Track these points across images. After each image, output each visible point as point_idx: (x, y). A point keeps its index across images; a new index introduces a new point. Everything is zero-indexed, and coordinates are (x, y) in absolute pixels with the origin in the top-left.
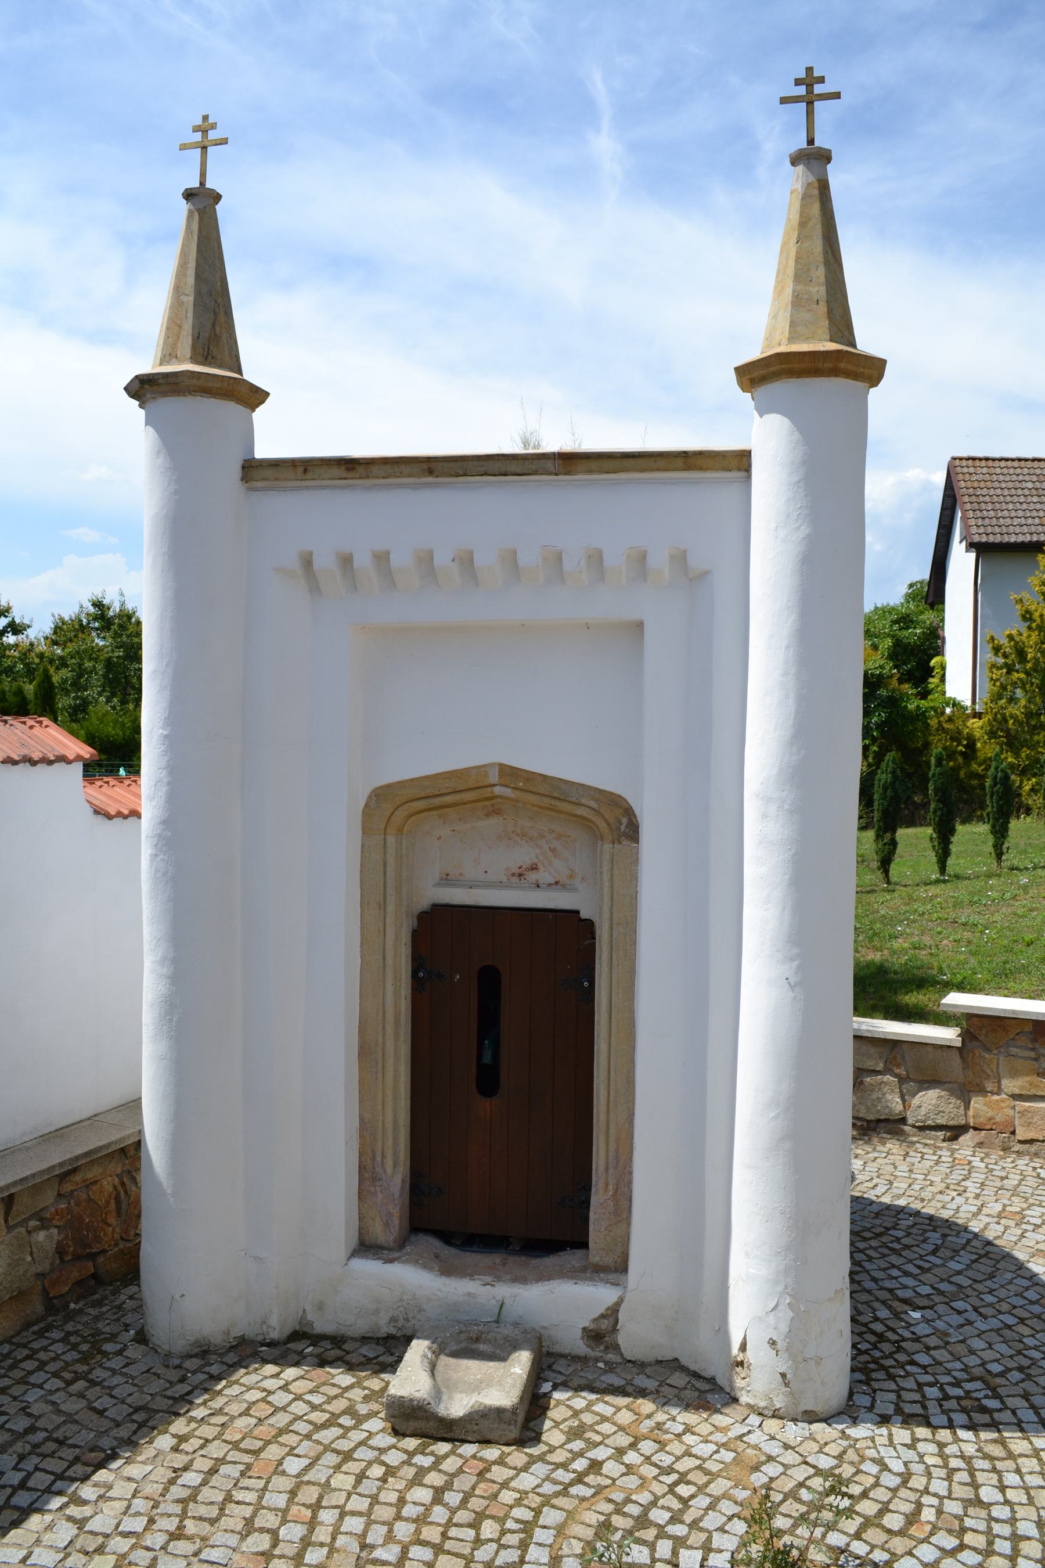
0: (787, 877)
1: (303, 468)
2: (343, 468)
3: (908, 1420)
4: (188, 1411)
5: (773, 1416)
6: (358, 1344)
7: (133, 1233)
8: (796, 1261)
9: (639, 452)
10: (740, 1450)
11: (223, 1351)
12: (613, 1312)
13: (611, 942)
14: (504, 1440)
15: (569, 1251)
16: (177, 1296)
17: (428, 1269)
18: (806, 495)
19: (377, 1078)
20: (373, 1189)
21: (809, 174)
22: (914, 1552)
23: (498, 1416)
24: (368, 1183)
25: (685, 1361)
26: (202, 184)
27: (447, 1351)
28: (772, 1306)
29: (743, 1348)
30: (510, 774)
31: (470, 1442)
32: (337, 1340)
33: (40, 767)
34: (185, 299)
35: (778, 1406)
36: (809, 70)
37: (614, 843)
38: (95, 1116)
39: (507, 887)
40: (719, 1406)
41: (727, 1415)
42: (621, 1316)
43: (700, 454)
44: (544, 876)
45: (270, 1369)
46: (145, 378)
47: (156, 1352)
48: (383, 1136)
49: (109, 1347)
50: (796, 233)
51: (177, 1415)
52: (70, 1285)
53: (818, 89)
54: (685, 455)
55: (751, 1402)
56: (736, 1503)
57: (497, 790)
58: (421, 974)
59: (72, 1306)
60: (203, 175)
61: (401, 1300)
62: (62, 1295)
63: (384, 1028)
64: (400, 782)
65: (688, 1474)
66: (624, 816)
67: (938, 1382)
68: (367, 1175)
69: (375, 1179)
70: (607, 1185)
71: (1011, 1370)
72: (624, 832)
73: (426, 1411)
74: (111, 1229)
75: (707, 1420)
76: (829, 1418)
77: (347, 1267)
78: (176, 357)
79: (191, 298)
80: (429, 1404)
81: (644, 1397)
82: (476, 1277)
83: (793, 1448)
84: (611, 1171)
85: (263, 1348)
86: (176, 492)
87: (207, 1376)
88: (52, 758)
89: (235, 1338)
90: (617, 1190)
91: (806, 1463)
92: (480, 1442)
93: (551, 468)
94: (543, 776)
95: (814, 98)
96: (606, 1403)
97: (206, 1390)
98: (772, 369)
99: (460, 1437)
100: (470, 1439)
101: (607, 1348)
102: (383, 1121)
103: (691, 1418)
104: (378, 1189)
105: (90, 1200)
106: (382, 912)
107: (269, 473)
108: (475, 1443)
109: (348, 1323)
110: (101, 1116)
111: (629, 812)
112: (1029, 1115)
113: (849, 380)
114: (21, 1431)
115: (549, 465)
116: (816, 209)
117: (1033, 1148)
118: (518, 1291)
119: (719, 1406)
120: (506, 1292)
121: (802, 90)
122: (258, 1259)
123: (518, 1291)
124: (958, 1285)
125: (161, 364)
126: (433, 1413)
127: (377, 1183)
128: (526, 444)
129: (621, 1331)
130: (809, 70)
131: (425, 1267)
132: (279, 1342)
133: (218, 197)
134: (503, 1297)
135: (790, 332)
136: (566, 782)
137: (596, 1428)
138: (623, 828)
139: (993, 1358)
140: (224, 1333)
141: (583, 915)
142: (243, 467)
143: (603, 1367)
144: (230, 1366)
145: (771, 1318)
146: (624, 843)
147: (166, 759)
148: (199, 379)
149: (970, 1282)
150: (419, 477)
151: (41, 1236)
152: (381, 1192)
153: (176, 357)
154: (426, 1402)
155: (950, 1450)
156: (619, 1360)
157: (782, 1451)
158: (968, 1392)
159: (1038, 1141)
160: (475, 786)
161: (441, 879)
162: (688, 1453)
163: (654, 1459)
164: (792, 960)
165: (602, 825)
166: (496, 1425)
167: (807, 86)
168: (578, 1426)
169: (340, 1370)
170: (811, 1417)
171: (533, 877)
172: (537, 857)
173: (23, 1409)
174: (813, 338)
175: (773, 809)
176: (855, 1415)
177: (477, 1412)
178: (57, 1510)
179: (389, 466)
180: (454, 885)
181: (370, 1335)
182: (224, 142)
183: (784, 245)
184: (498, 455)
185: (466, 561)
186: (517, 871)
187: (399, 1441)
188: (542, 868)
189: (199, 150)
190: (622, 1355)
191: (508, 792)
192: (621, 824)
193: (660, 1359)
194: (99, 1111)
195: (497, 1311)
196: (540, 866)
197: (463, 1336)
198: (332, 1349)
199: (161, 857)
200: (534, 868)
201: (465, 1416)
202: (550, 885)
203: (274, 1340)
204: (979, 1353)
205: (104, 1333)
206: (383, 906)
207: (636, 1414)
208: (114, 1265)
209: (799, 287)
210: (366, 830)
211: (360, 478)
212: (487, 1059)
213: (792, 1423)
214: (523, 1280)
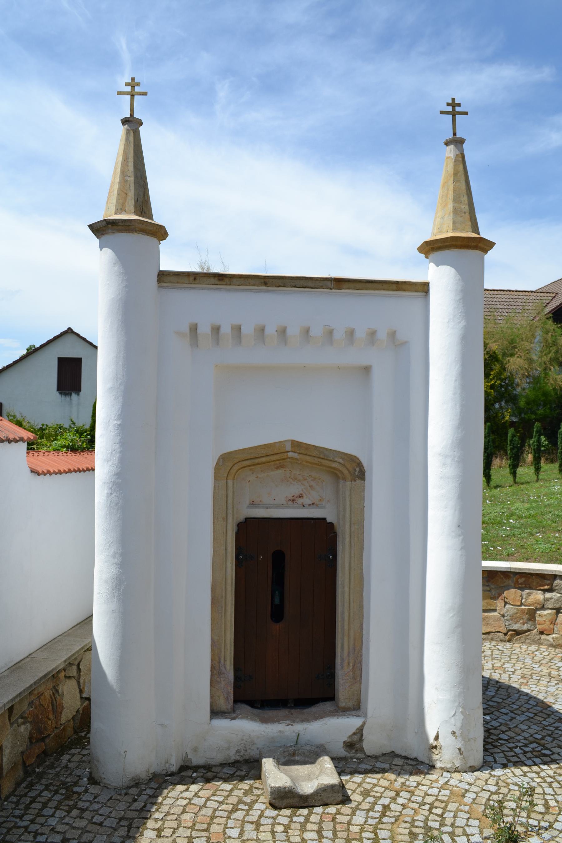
0: (457, 494)
1: (194, 277)
3: (516, 764)
4: (151, 816)
5: (455, 771)
6: (220, 768)
9: (375, 280)
10: (450, 789)
12: (360, 731)
13: (350, 533)
14: (335, 802)
16: (122, 753)
17: (254, 721)
19: (222, 616)
20: (219, 680)
21: (457, 150)
22: (558, 819)
23: (332, 789)
25: (398, 752)
26: (132, 115)
27: (281, 763)
28: (453, 713)
29: (437, 738)
30: (297, 445)
31: (317, 806)
32: (207, 768)
33: (13, 443)
34: (128, 179)
35: (457, 765)
37: (351, 481)
39: (287, 507)
43: (405, 283)
44: (306, 501)
46: (111, 221)
47: (108, 788)
50: (452, 178)
54: (397, 283)
55: (443, 766)
57: (290, 454)
58: (241, 557)
59: (37, 770)
60: (132, 110)
61: (242, 740)
63: (226, 588)
64: (236, 451)
65: (433, 803)
66: (357, 467)
68: (215, 672)
69: (220, 673)
70: (349, 663)
71: (545, 736)
72: (357, 475)
73: (293, 793)
74: (50, 722)
75: (424, 778)
76: (480, 768)
78: (125, 211)
80: (294, 789)
81: (387, 772)
82: (281, 722)
83: (473, 784)
84: (351, 655)
85: (168, 778)
87: (148, 796)
88: (18, 439)
89: (151, 774)
91: (484, 790)
92: (323, 805)
93: (330, 286)
95: (456, 113)
96: (370, 777)
99: (311, 805)
100: (317, 804)
101: (357, 751)
103: (418, 778)
104: (222, 679)
106: (225, 523)
107: (173, 279)
108: (320, 806)
109: (212, 757)
111: (360, 464)
112: (487, 619)
115: (329, 284)
116: (461, 167)
117: (490, 636)
119: (426, 771)
120: (299, 727)
122: (163, 726)
125: (115, 214)
126: (296, 793)
127: (222, 676)
128: (202, 267)
130: (453, 99)
131: (252, 719)
132: (175, 773)
135: (453, 227)
138: (357, 473)
139: (534, 732)
140: (147, 771)
141: (329, 520)
142: (158, 275)
143: (356, 761)
144: (156, 789)
145: (453, 720)
147: (119, 438)
148: (143, 224)
150: (258, 286)
151: (22, 728)
152: (224, 680)
153: (125, 211)
154: (292, 788)
155: (543, 774)
156: (364, 756)
157: (469, 787)
158: (533, 749)
159: (492, 632)
160: (278, 452)
161: (250, 504)
162: (426, 794)
164: (460, 536)
165: (346, 472)
166: (331, 795)
167: (452, 107)
168: (364, 790)
170: (473, 769)
171: (300, 501)
174: (464, 230)
175: (449, 461)
176: (491, 766)
177: (320, 789)
179: (242, 279)
181: (225, 762)
185: (283, 332)
186: (292, 498)
187: (279, 812)
190: (365, 753)
191: (296, 455)
192: (356, 471)
193: (384, 753)
194: (32, 652)
195: (296, 739)
196: (304, 495)
197: (286, 754)
198: (207, 772)
199: (115, 494)
200: (301, 496)
201: (314, 792)
202: (309, 505)
203: (173, 772)
205: (68, 782)
206: (226, 519)
207: (388, 780)
208: (53, 744)
209: (456, 205)
211: (226, 285)
212: (277, 601)
213: (465, 773)
214: (307, 720)
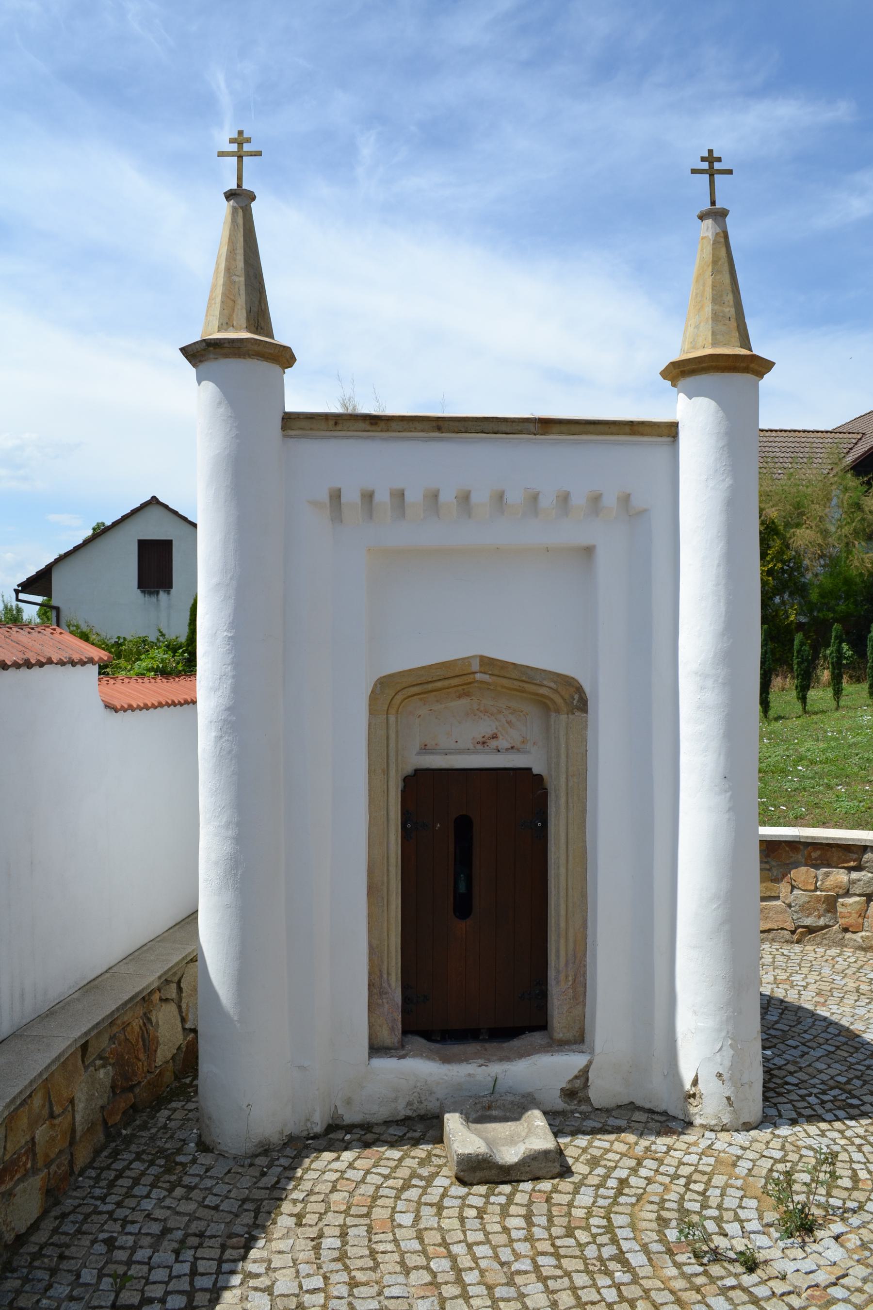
0: (722, 731)
2: (368, 422)
5: (722, 1130)
6: (384, 1128)
7: (153, 1066)
8: (733, 1012)
11: (279, 1148)
12: (584, 1074)
13: (567, 789)
14: (550, 1175)
15: (528, 1034)
16: (244, 1107)
18: (729, 457)
19: (383, 911)
23: (546, 1157)
24: (376, 997)
25: (639, 1103)
27: (471, 1119)
28: (718, 1048)
29: (695, 1083)
30: (488, 663)
31: (524, 1181)
33: (79, 666)
34: (236, 279)
35: (725, 1122)
36: (711, 152)
38: (109, 969)
39: (474, 752)
40: (680, 1130)
41: (690, 1134)
42: (590, 1074)
44: (503, 743)
45: (328, 1156)
46: (213, 342)
48: (388, 958)
49: (180, 1159)
51: (281, 1200)
52: (120, 1114)
53: (717, 165)
54: (631, 424)
55: (704, 1123)
56: (738, 1188)
57: (478, 676)
58: (409, 826)
59: (124, 1132)
61: (415, 1087)
62: (116, 1124)
67: (812, 1093)
69: (382, 993)
70: (567, 977)
72: (576, 705)
73: (489, 1162)
75: (678, 1140)
77: (369, 1066)
78: (233, 326)
79: (242, 279)
80: (491, 1156)
84: (571, 966)
85: (310, 1142)
86: (237, 436)
87: (282, 1168)
90: (575, 980)
91: (764, 1156)
92: (532, 1180)
93: (533, 429)
94: (514, 664)
96: (599, 1139)
97: (290, 1179)
98: (703, 365)
100: (523, 1178)
101: (580, 1101)
102: (388, 946)
103: (668, 1140)
104: (384, 1001)
105: (127, 1039)
108: (528, 1181)
109: (372, 1112)
110: (114, 968)
111: (580, 690)
113: (753, 376)
114: (159, 1233)
115: (531, 427)
116: (723, 252)
118: (508, 1067)
119: (680, 1130)
120: (496, 1069)
121: (705, 165)
122: (302, 1068)
123: (508, 1067)
124: (781, 1030)
125: (219, 331)
126: (494, 1163)
127: (384, 996)
129: (591, 1087)
130: (711, 152)
131: (428, 1058)
133: (252, 197)
134: (497, 1073)
136: (532, 669)
137: (605, 1157)
138: (575, 702)
142: (283, 419)
143: (579, 1116)
144: (294, 1158)
145: (718, 1058)
146: (576, 714)
147: (231, 656)
149: (788, 1027)
152: (388, 1003)
153: (233, 326)
156: (590, 1109)
157: (743, 1152)
160: (461, 674)
162: (681, 1163)
163: (660, 1170)
164: (726, 791)
165: (559, 701)
169: (386, 1148)
170: (748, 1127)
171: (493, 744)
172: (497, 729)
173: (148, 1216)
174: (728, 344)
175: (709, 683)
176: (773, 1122)
177: (529, 1156)
178: (240, 1285)
180: (432, 754)
182: (258, 154)
183: (700, 276)
184: (493, 418)
186: (481, 740)
187: (470, 1190)
188: (501, 737)
189: (236, 158)
190: (591, 1105)
191: (486, 678)
192: (574, 699)
196: (499, 735)
197: (478, 1106)
200: (494, 737)
202: (507, 749)
204: (825, 1071)
206: (387, 772)
207: (626, 1144)
208: (145, 1095)
209: (716, 307)
210: (372, 712)
211: (381, 431)
212: (462, 888)
214: (508, 1059)
